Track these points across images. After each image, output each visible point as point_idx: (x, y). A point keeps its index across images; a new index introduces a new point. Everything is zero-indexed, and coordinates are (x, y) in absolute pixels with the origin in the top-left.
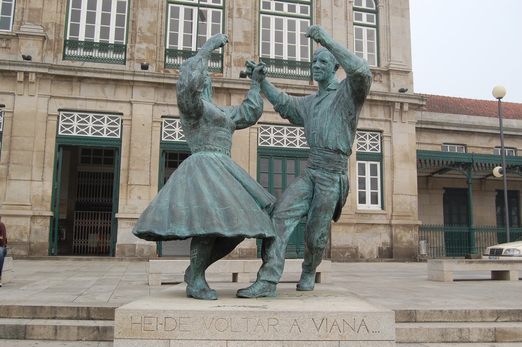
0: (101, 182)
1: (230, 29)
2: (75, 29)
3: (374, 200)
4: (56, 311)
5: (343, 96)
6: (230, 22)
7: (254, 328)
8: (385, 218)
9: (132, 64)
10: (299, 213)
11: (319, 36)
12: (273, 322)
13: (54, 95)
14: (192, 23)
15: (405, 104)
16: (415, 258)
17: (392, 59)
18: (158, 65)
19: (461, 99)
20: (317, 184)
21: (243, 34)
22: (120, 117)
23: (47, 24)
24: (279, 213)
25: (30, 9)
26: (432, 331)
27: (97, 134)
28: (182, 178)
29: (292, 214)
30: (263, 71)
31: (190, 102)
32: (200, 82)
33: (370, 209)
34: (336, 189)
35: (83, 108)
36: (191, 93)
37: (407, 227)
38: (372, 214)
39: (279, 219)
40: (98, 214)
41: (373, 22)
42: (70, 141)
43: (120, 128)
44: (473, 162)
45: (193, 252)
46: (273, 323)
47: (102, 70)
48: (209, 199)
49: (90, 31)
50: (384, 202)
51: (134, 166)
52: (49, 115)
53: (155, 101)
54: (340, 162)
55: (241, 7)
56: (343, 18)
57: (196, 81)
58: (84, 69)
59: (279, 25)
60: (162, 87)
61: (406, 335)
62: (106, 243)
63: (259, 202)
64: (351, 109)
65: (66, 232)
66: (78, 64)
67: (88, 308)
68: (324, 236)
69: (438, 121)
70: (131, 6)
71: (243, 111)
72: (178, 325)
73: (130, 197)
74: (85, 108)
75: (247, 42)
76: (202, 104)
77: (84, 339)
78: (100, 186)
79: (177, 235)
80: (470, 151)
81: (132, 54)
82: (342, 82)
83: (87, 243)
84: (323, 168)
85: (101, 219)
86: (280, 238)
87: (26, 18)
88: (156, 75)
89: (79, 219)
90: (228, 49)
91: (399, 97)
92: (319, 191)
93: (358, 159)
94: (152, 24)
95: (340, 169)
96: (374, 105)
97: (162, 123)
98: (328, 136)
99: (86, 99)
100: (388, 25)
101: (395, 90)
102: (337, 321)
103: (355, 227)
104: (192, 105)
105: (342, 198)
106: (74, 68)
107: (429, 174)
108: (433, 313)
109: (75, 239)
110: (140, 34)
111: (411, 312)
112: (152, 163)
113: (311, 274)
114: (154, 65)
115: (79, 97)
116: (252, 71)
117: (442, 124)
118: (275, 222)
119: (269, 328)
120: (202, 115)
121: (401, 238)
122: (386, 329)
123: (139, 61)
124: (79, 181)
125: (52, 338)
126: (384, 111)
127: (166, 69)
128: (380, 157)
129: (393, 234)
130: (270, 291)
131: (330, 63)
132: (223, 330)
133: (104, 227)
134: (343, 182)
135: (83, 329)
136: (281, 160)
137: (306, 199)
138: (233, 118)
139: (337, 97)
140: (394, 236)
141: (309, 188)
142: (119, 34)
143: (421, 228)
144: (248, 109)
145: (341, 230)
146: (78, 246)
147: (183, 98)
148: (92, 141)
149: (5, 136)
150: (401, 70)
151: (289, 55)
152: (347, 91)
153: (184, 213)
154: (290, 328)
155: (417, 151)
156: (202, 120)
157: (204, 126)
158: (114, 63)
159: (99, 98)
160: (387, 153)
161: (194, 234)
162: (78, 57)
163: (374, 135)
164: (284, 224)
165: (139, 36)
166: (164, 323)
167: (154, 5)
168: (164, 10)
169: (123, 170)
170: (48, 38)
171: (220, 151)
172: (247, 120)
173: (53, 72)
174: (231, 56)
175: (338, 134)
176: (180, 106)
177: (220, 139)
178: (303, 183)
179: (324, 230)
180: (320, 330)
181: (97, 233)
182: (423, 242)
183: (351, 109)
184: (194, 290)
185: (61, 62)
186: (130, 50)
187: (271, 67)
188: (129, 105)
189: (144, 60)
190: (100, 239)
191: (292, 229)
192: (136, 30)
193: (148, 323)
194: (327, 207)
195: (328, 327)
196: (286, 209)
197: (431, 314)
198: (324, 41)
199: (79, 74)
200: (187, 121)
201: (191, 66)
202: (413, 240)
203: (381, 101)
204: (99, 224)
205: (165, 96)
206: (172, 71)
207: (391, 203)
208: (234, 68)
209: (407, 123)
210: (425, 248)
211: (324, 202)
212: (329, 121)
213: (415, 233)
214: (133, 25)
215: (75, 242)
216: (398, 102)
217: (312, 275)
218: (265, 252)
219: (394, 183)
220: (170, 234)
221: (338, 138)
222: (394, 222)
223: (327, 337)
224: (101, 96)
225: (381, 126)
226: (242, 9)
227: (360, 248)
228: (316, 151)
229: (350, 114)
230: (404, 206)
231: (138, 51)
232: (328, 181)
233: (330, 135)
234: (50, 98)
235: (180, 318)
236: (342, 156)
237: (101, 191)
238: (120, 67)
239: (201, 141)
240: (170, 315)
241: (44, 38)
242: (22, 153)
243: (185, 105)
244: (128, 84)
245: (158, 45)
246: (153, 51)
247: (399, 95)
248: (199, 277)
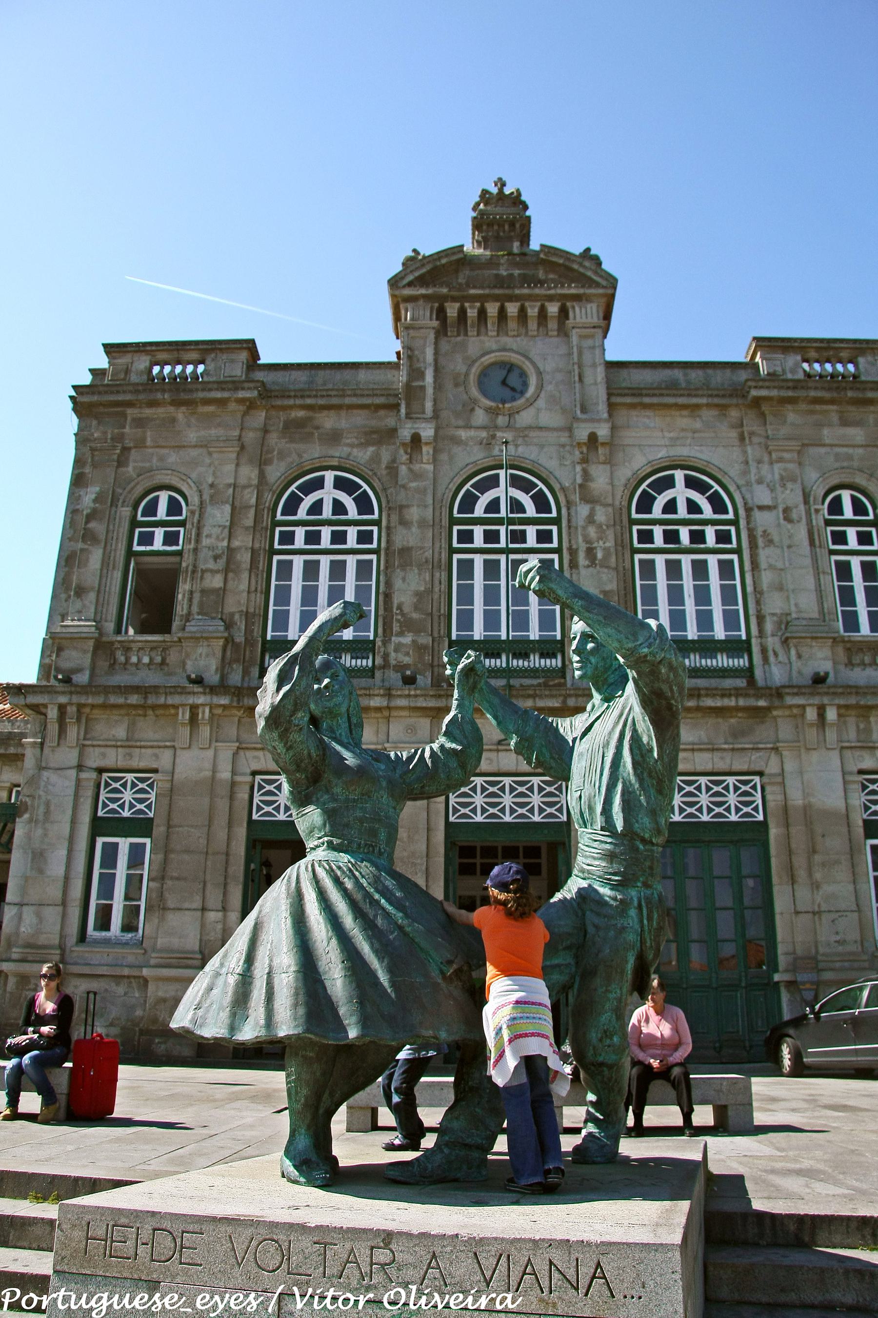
23: (232, 615)
25: (203, 591)
55: (594, 545)
56: (806, 543)
59: (674, 569)
70: (382, 567)
81: (386, 656)
87: (195, 609)
110: (399, 617)
114: (428, 674)
123: (400, 668)
132: (271, 1268)
149: (158, 826)
151: (700, 628)
154: (422, 1273)
165: (398, 621)
168: (443, 567)
186: (382, 649)
187: (692, 656)
189: (407, 666)
192: (392, 611)
193: (119, 1239)
226: (595, 548)
235: (183, 1232)
240: (167, 1224)
242: (186, 857)
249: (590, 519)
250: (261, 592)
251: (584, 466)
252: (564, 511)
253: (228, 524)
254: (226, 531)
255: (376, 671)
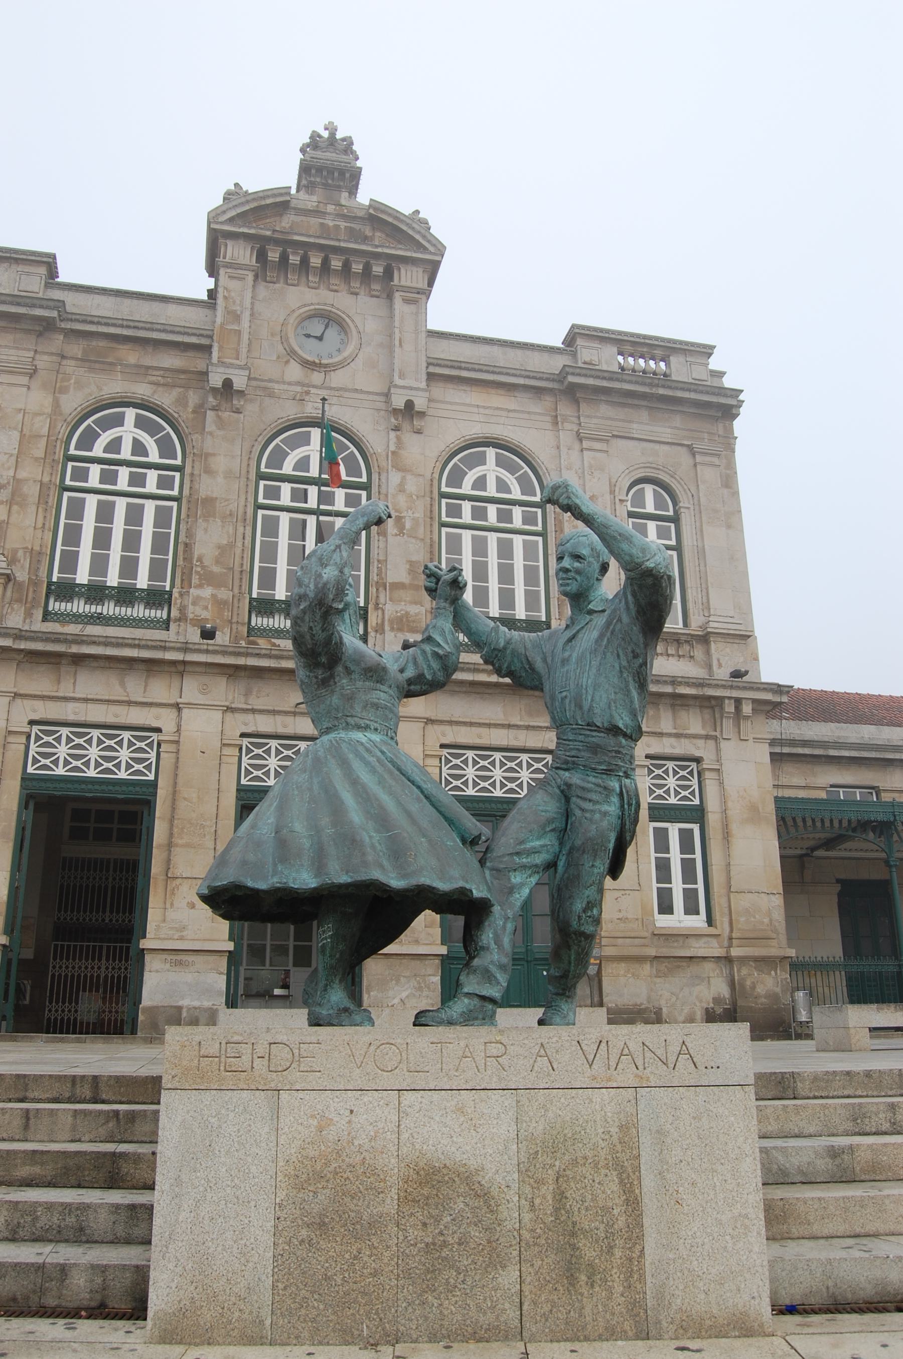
0: (110, 879)
1: (381, 558)
2: (70, 561)
3: (691, 909)
4: (27, 1085)
5: (620, 620)
6: (382, 545)
7: (457, 1062)
8: (716, 945)
9: (182, 628)
10: (539, 859)
11: (569, 498)
12: (494, 1049)
13: (22, 692)
14: (304, 546)
15: (744, 702)
16: (785, 1031)
17: (712, 612)
18: (234, 630)
19: (860, 695)
20: (574, 799)
21: (408, 567)
22: (155, 736)
23: (15, 551)
24: (499, 857)
26: (832, 1111)
27: (108, 771)
28: (300, 779)
29: (524, 860)
30: (459, 583)
31: (317, 629)
32: (337, 589)
33: (682, 925)
34: (613, 808)
35: (81, 718)
36: (320, 609)
37: (765, 963)
38: (687, 936)
39: (498, 870)
40: (101, 948)
41: (671, 539)
42: (50, 785)
43: (154, 760)
44: (895, 820)
45: (324, 932)
46: (495, 1052)
47: (121, 641)
48: (355, 815)
49: (99, 564)
50: (713, 909)
51: (182, 838)
52: (10, 732)
53: (227, 704)
54: (619, 752)
57: (330, 586)
58: (85, 638)
60: (243, 674)
61: (776, 1120)
62: (117, 1012)
63: (456, 828)
64: (636, 644)
65: (31, 987)
66: (73, 629)
67: (95, 1078)
68: (593, 907)
69: (816, 738)
71: (420, 659)
72: (297, 1058)
73: (172, 905)
74: (83, 719)
75: (416, 583)
76: (341, 638)
77: (87, 1138)
78: (106, 887)
79: (292, 885)
80: (886, 797)
81: (182, 609)
82: (616, 596)
83: (76, 1011)
84: (584, 766)
85: (108, 960)
86: (502, 909)
88: (231, 649)
89: (61, 959)
90: (377, 597)
91: (731, 687)
92: (578, 813)
93: (653, 819)
94: (224, 550)
95: (620, 767)
96: (682, 705)
97: (241, 749)
98: (592, 700)
99: (86, 700)
100: (700, 545)
101: (722, 673)
102: (631, 1045)
103: (652, 966)
104: (321, 636)
105: (627, 827)
106: (65, 637)
107: (804, 852)
108: (831, 1077)
109: (51, 1003)
111: (783, 1078)
112: (219, 832)
113: (569, 997)
114: (227, 630)
115: (72, 695)
116: (437, 583)
117: (824, 744)
118: (491, 875)
119: (488, 1064)
120: (341, 659)
121: (753, 987)
122: (734, 1061)
123: (197, 622)
124: (63, 877)
125: (17, 1137)
126: (703, 718)
127: (251, 638)
128: (698, 814)
129: (736, 978)
130: (484, 1019)
131: (591, 559)
133: (113, 977)
134: (627, 792)
135: (85, 1115)
136: (491, 824)
137: (553, 830)
138: (402, 671)
139: (608, 624)
140: (739, 983)
141: (558, 808)
142: (157, 570)
143: (797, 967)
144: (429, 655)
145: (622, 972)
146: (56, 1019)
147: (303, 620)
148: (97, 787)
150: (732, 632)
152: (628, 608)
153: (306, 843)
154: (532, 1062)
155: (776, 797)
156: (340, 669)
157: (344, 681)
158: (145, 628)
159: (111, 698)
160: (713, 805)
161: (327, 884)
162: (74, 615)
163: (683, 768)
164: (509, 879)
165: (197, 572)
166: (267, 1055)
167: (228, 513)
168: (248, 522)
169: (159, 846)
170: (15, 578)
171: (376, 730)
172: (429, 677)
173: (23, 645)
174: (383, 611)
175: (613, 696)
176: (298, 641)
177: (376, 706)
178: (545, 799)
179: (591, 892)
180: (594, 1066)
181: (97, 991)
182: (800, 995)
183: (636, 644)
184: (324, 1012)
185: (38, 626)
186: (179, 601)
187: (277, 617)
188: (174, 711)
190: (104, 1003)
191: (526, 892)
193: (233, 1055)
194: (597, 844)
195: (611, 1060)
196: (511, 851)
197: (827, 1081)
198: (577, 507)
199: (75, 649)
200: (310, 671)
201: (320, 559)
202: (778, 990)
203: (695, 697)
204: (103, 969)
205: (247, 694)
206: (263, 643)
207: (726, 911)
208: (389, 636)
209: (751, 740)
210: (807, 1008)
211: (590, 835)
212: (594, 671)
213: (784, 975)
214: (185, 551)
215: (50, 1011)
216: (730, 698)
217: (569, 1000)
218: (471, 936)
219: (732, 867)
220: (278, 885)
221: (613, 704)
222: (735, 952)
223: (609, 1080)
224: (117, 693)
225: (698, 748)
227: (665, 1010)
228: (569, 734)
229: (636, 656)
230: (755, 917)
231: (194, 604)
232: (596, 791)
233: (597, 698)
234: (14, 697)
236: (623, 741)
237: (109, 899)
238: (158, 635)
239: (337, 710)
241: (8, 578)
243: (308, 637)
244: (173, 669)
245: (236, 591)
246: (225, 603)
247: (730, 683)
248: (335, 986)
249: (401, 489)
250: (49, 530)
251: (398, 433)
252: (375, 477)
253: (16, 452)
254: (14, 459)
255: (171, 623)
